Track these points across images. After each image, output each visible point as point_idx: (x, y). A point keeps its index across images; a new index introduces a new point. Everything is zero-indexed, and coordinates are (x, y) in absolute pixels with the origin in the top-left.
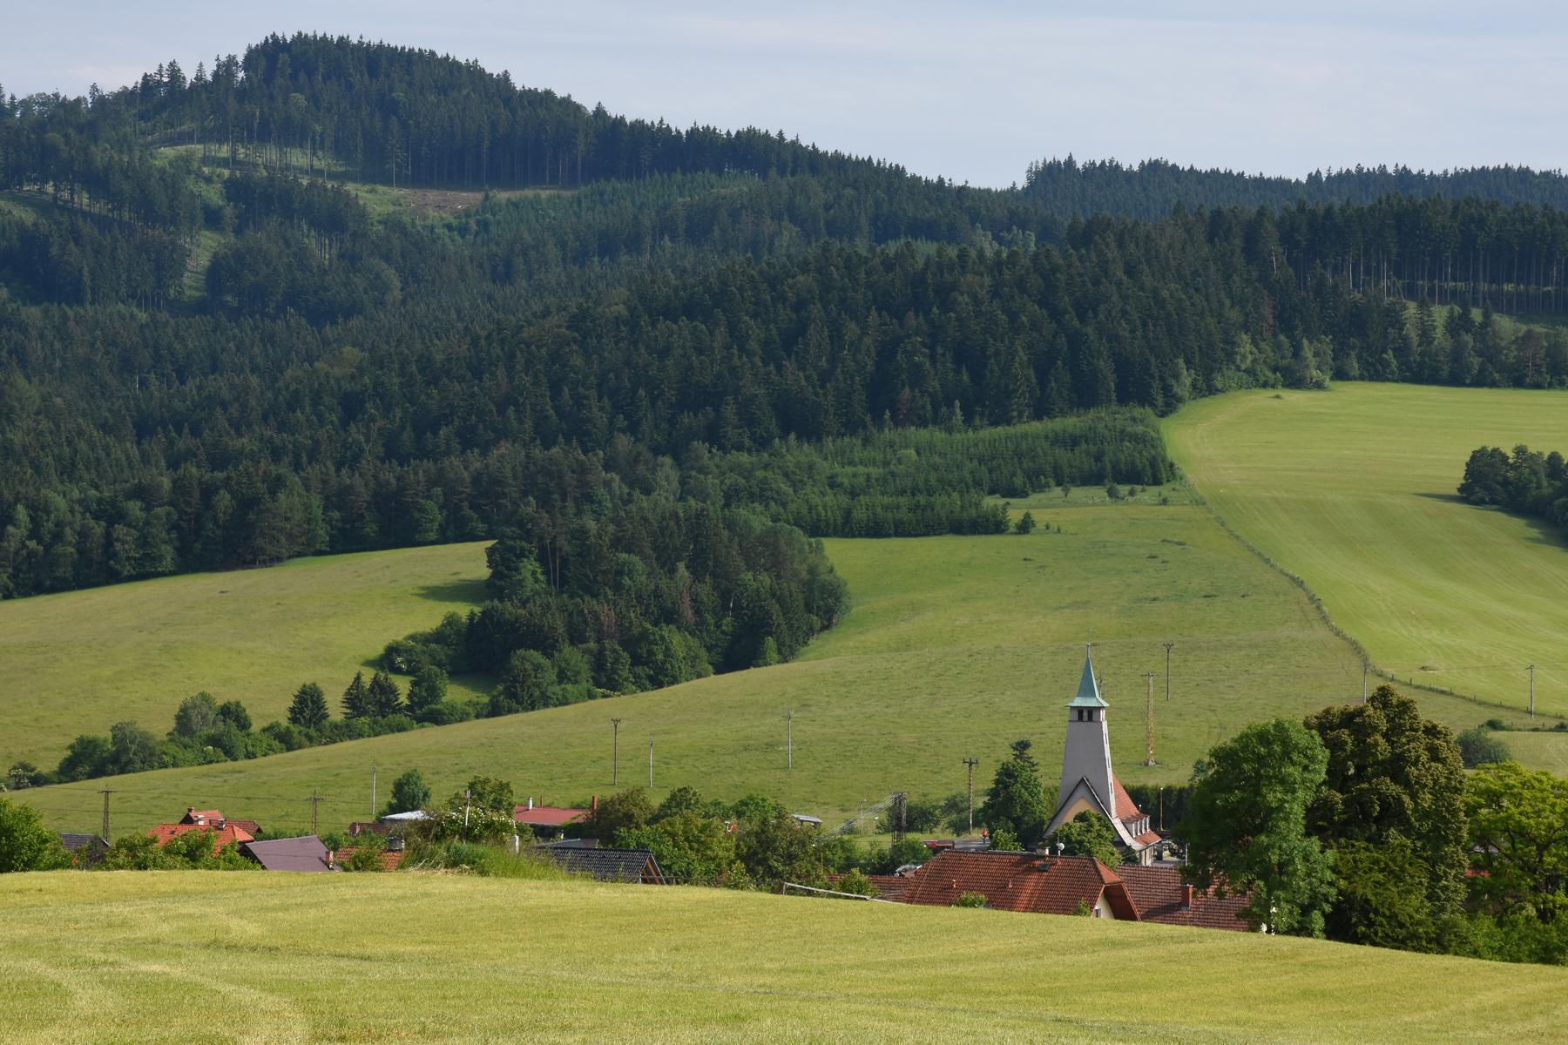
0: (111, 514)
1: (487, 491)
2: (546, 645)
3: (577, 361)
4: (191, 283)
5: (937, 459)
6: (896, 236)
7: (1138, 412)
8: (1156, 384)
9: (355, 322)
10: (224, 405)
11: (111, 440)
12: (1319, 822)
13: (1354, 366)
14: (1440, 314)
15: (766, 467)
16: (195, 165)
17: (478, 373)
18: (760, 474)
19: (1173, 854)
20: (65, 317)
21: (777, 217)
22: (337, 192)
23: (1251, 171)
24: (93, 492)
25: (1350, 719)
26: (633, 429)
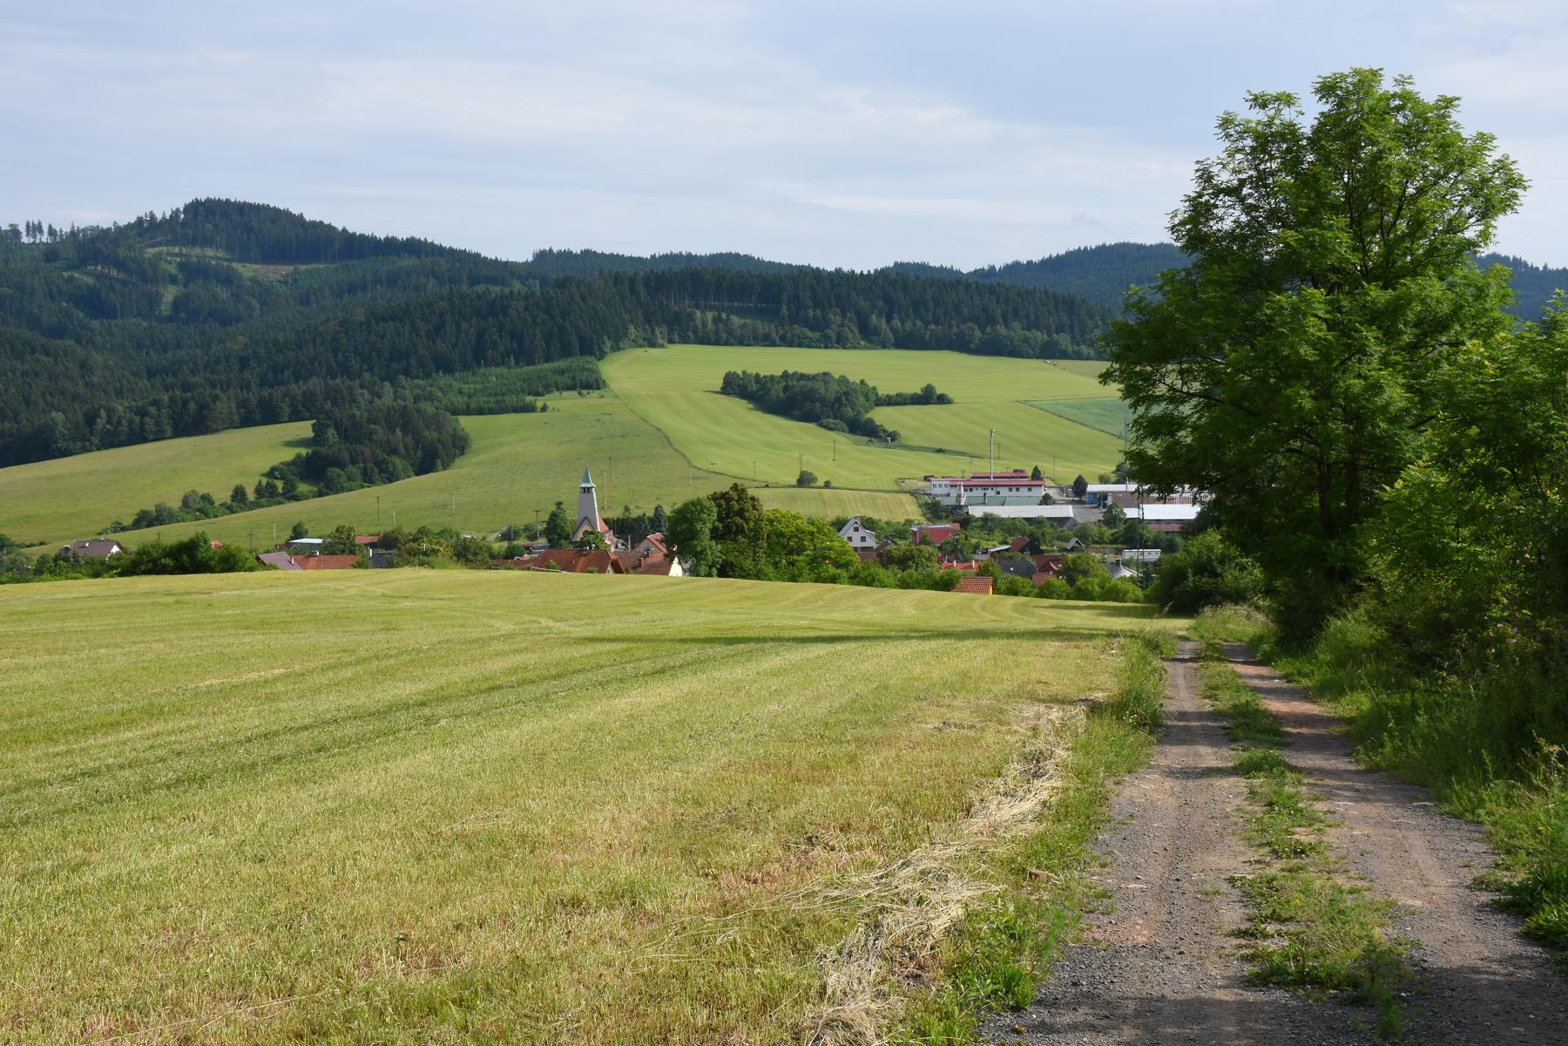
0: (142, 413)
1: (309, 398)
2: (342, 466)
3: (344, 341)
4: (165, 308)
5: (505, 381)
6: (479, 283)
7: (589, 359)
8: (596, 347)
9: (241, 325)
10: (186, 363)
11: (137, 379)
12: (716, 535)
13: (676, 338)
14: (710, 315)
15: (431, 386)
16: (164, 257)
17: (300, 347)
18: (429, 389)
19: (623, 545)
20: (110, 324)
21: (426, 276)
22: (228, 267)
23: (627, 254)
24: (134, 403)
25: (724, 496)
26: (370, 370)
